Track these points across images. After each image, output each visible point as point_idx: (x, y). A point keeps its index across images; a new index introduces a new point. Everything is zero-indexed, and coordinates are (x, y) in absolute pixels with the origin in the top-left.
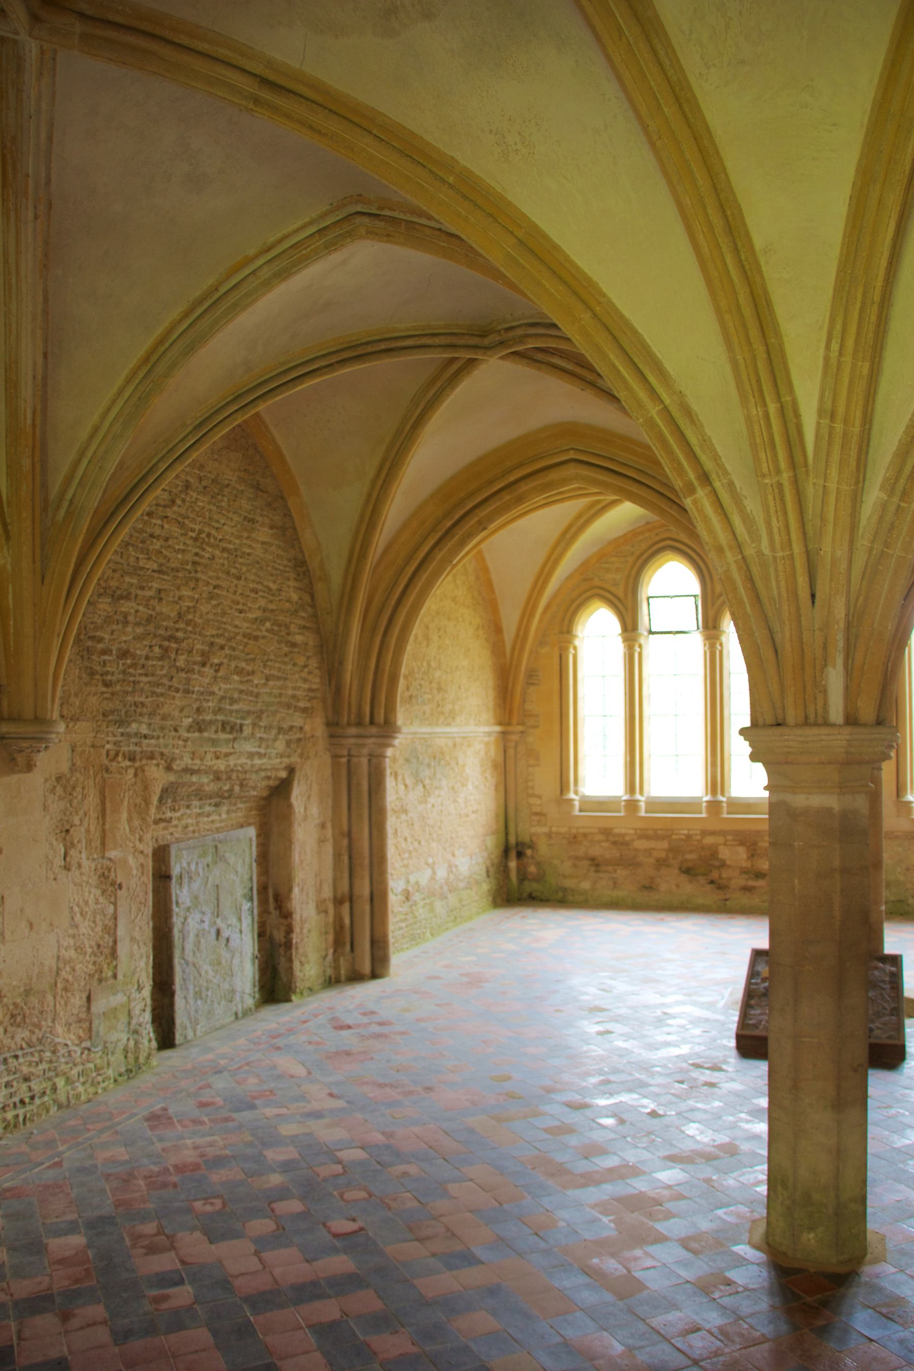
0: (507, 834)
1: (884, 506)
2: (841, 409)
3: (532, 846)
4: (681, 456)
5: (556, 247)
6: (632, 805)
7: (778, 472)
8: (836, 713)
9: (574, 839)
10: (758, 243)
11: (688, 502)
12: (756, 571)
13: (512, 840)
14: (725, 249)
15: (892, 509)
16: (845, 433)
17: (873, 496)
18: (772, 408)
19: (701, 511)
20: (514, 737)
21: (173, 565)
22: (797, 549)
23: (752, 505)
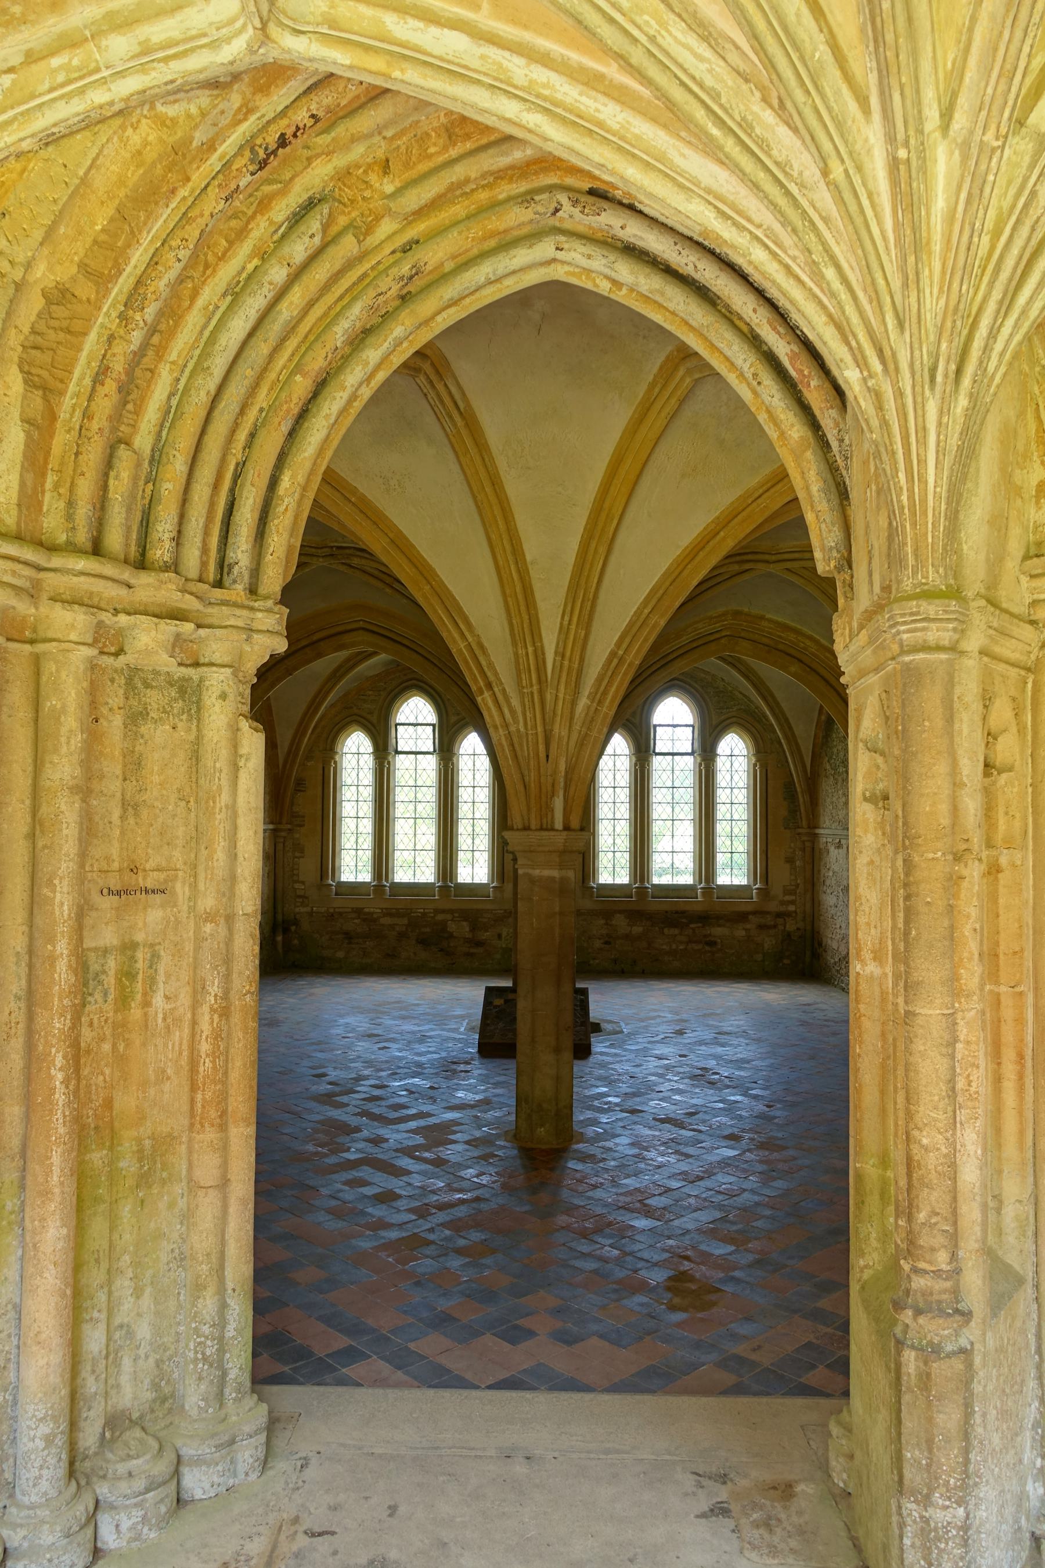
0: (275, 913)
1: (589, 707)
2: (568, 654)
3: (296, 922)
5: (413, 546)
6: (379, 888)
7: (532, 686)
8: (559, 824)
9: (331, 916)
10: (529, 558)
11: (479, 699)
12: (515, 740)
13: (280, 917)
15: (593, 709)
16: (570, 667)
17: (583, 702)
18: (530, 649)
19: (486, 704)
20: (283, 834)
22: (540, 729)
23: (515, 702)
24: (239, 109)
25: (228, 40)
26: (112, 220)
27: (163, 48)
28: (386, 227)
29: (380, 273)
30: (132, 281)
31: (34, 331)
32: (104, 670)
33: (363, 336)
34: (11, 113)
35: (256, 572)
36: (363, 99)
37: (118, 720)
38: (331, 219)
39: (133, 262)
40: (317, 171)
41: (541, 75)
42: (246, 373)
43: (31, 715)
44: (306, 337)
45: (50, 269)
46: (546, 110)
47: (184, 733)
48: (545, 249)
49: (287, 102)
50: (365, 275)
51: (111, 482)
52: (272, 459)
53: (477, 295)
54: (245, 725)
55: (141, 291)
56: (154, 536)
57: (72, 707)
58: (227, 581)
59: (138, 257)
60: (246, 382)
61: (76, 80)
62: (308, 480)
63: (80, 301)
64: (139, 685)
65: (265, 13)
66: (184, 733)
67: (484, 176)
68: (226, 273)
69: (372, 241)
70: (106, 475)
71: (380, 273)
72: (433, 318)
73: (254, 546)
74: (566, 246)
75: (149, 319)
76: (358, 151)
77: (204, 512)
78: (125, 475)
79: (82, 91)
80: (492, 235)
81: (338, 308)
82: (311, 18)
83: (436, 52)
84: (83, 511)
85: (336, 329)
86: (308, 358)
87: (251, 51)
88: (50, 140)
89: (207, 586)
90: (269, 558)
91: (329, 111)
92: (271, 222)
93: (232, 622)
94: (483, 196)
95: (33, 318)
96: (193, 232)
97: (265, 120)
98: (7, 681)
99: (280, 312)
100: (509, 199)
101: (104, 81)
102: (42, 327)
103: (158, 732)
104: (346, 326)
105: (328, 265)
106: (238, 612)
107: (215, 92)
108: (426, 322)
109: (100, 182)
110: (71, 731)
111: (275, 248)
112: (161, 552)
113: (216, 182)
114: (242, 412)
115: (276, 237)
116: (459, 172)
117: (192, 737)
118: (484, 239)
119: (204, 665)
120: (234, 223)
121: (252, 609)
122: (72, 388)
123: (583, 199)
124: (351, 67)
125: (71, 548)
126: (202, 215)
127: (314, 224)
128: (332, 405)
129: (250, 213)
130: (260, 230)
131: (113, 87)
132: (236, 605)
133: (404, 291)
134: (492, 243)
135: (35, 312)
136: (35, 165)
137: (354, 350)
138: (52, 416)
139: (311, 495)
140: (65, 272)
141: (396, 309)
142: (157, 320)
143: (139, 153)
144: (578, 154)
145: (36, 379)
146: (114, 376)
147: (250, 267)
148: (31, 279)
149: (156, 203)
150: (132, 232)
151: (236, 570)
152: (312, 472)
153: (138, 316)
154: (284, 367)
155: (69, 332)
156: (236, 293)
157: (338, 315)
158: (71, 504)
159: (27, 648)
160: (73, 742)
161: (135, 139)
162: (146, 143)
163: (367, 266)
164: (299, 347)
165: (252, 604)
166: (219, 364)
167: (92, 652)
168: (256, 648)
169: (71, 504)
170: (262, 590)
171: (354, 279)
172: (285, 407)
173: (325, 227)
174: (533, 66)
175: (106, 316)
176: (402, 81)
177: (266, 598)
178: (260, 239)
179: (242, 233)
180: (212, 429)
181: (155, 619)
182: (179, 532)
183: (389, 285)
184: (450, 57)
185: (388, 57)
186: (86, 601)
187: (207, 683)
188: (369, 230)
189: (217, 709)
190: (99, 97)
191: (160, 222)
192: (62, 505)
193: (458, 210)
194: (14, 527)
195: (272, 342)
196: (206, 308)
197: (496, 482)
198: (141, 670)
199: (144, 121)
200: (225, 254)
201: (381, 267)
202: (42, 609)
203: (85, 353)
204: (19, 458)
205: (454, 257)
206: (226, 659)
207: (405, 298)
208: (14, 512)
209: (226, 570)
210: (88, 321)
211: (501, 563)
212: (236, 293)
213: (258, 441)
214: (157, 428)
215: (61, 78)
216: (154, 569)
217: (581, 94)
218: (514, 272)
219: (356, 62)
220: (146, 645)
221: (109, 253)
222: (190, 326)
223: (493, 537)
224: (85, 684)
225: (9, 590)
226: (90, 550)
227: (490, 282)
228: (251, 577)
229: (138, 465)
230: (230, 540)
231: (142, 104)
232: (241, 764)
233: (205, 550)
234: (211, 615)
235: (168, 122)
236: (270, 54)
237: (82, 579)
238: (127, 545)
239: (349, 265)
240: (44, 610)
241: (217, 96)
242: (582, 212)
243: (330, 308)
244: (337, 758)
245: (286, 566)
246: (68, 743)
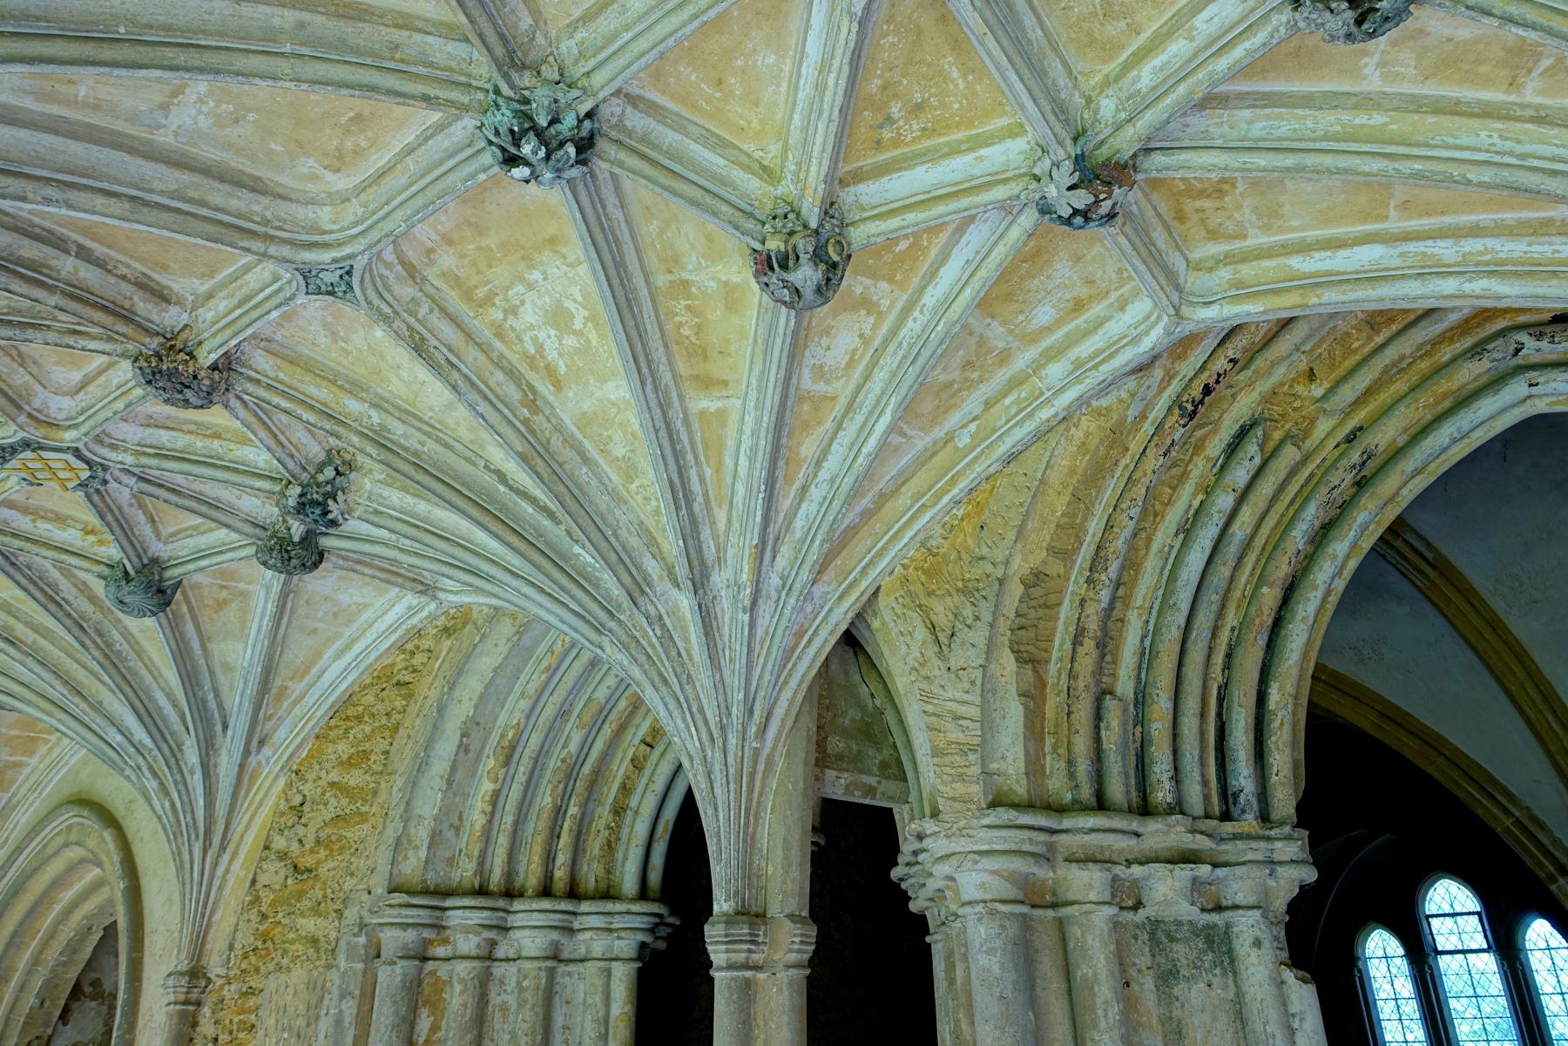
4: (1538, 854)
5: (1408, 714)
14: (1546, 713)
21: (844, 362)
24: (1163, 379)
25: (1147, 333)
26: (1069, 504)
27: (1091, 358)
28: (1322, 427)
29: (1328, 469)
30: (1093, 547)
31: (1018, 615)
32: (1125, 926)
33: (1324, 532)
34: (979, 449)
35: (1263, 795)
36: (1275, 329)
37: (1149, 982)
38: (1266, 436)
39: (1091, 531)
40: (1242, 403)
41: (1473, 245)
42: (1211, 598)
43: (1064, 986)
44: (1264, 548)
45: (1025, 559)
46: (1490, 272)
47: (1222, 992)
48: (1517, 388)
49: (1205, 358)
50: (1312, 475)
51: (1103, 733)
52: (1256, 675)
53: (1443, 457)
54: (1289, 975)
55: (1102, 554)
56: (1153, 778)
57: (1103, 974)
58: (1235, 812)
59: (1095, 527)
60: (1214, 608)
61: (1026, 407)
62: (1298, 687)
63: (1053, 578)
64: (1163, 939)
65: (1176, 302)
66: (1222, 992)
67: (1419, 348)
68: (1174, 516)
69: (1309, 444)
70: (1097, 727)
71: (1328, 469)
72: (1397, 493)
73: (1256, 768)
74: (1541, 380)
75: (1113, 576)
76: (1279, 373)
77: (1196, 744)
78: (1115, 724)
79: (1031, 415)
80: (1445, 396)
81: (1291, 513)
82: (1219, 289)
83: (1349, 270)
84: (1083, 767)
85: (1294, 533)
86: (1271, 568)
87: (1168, 333)
88: (1011, 458)
89: (1215, 822)
90: (1274, 779)
91: (1245, 351)
92: (1208, 459)
93: (1250, 856)
94: (1424, 365)
95: (1016, 604)
96: (1139, 491)
97: (1187, 379)
98: (1037, 951)
99: (1233, 535)
100: (1454, 359)
101: (1048, 400)
102: (1024, 609)
103: (1193, 991)
104: (1304, 527)
105: (1272, 479)
106: (1254, 845)
107: (1140, 374)
108: (1391, 500)
109: (1055, 477)
110: (1107, 1002)
111: (1217, 480)
112: (1162, 794)
113: (1153, 444)
114: (1214, 636)
115: (1215, 471)
116: (1391, 354)
117: (1231, 995)
118: (1437, 403)
119: (1227, 908)
120: (1174, 471)
121: (1269, 839)
122: (1055, 654)
123: (1548, 330)
124: (1265, 312)
125: (1078, 807)
126: (1145, 475)
127: (1251, 447)
128: (1308, 606)
129: (1187, 458)
130: (1199, 469)
131: (1055, 403)
132: (1249, 837)
133: (1359, 477)
134: (1447, 404)
135: (1017, 599)
136: (1002, 481)
137: (1317, 548)
138: (1042, 684)
139: (1304, 702)
140: (1037, 558)
141: (1354, 496)
142: (1120, 576)
143: (1084, 443)
144: (1545, 298)
145: (1025, 655)
146: (1091, 635)
147: (1196, 504)
148: (1010, 572)
149: (1104, 478)
150: (1087, 508)
151: (1242, 798)
152: (1300, 678)
153: (1103, 577)
154: (1248, 582)
155: (1047, 607)
156: (1187, 531)
157: (1293, 519)
158: (1071, 763)
159: (1050, 913)
160: (1110, 1015)
161: (1078, 434)
162: (1088, 434)
163: (1311, 467)
164: (1258, 560)
165: (1267, 833)
166: (1184, 598)
167: (1113, 910)
168: (1282, 882)
169: (1071, 763)
170: (1276, 815)
171: (1302, 481)
172: (1257, 621)
173: (1262, 447)
174: (1462, 243)
175: (1075, 585)
176: (1321, 304)
177: (1282, 823)
178: (1201, 477)
179: (1182, 478)
180: (1188, 660)
181: (1168, 866)
182: (1176, 768)
183: (1343, 478)
184: (1367, 268)
185: (1301, 291)
186: (1099, 856)
187: (1235, 929)
188: (1307, 433)
189: (1253, 959)
190: (1046, 413)
191: (1110, 490)
192: (1063, 764)
193: (1400, 386)
194: (1025, 796)
195: (1231, 563)
196: (1161, 551)
197: (1496, 625)
198: (1162, 921)
199: (1083, 418)
200: (1169, 501)
201: (1327, 463)
202: (1060, 872)
203: (1061, 621)
204: (1021, 730)
205: (1405, 430)
206: (1252, 900)
207: (1361, 484)
208: (1024, 782)
209: (1231, 800)
210: (1061, 592)
211: (1532, 716)
212: (1187, 531)
213: (1237, 660)
214: (1136, 672)
215: (1013, 410)
216: (1159, 814)
217: (1530, 245)
218: (1482, 423)
219: (1269, 306)
220: (1164, 895)
221: (1070, 531)
222: (1149, 570)
223: (1513, 688)
224: (1112, 947)
225: (1030, 859)
226: (1095, 804)
227: (1455, 441)
228: (1259, 802)
229: (1125, 710)
230: (1229, 767)
231: (1080, 407)
232: (1296, 1025)
233: (1205, 783)
234: (1226, 852)
235: (1104, 412)
236: (1188, 328)
237: (1093, 836)
238: (1128, 792)
239: (1293, 473)
240: (1061, 872)
241: (1142, 378)
242: (1552, 342)
243: (1282, 516)
244: (1360, 964)
245: (1296, 784)
246: (1106, 1015)
